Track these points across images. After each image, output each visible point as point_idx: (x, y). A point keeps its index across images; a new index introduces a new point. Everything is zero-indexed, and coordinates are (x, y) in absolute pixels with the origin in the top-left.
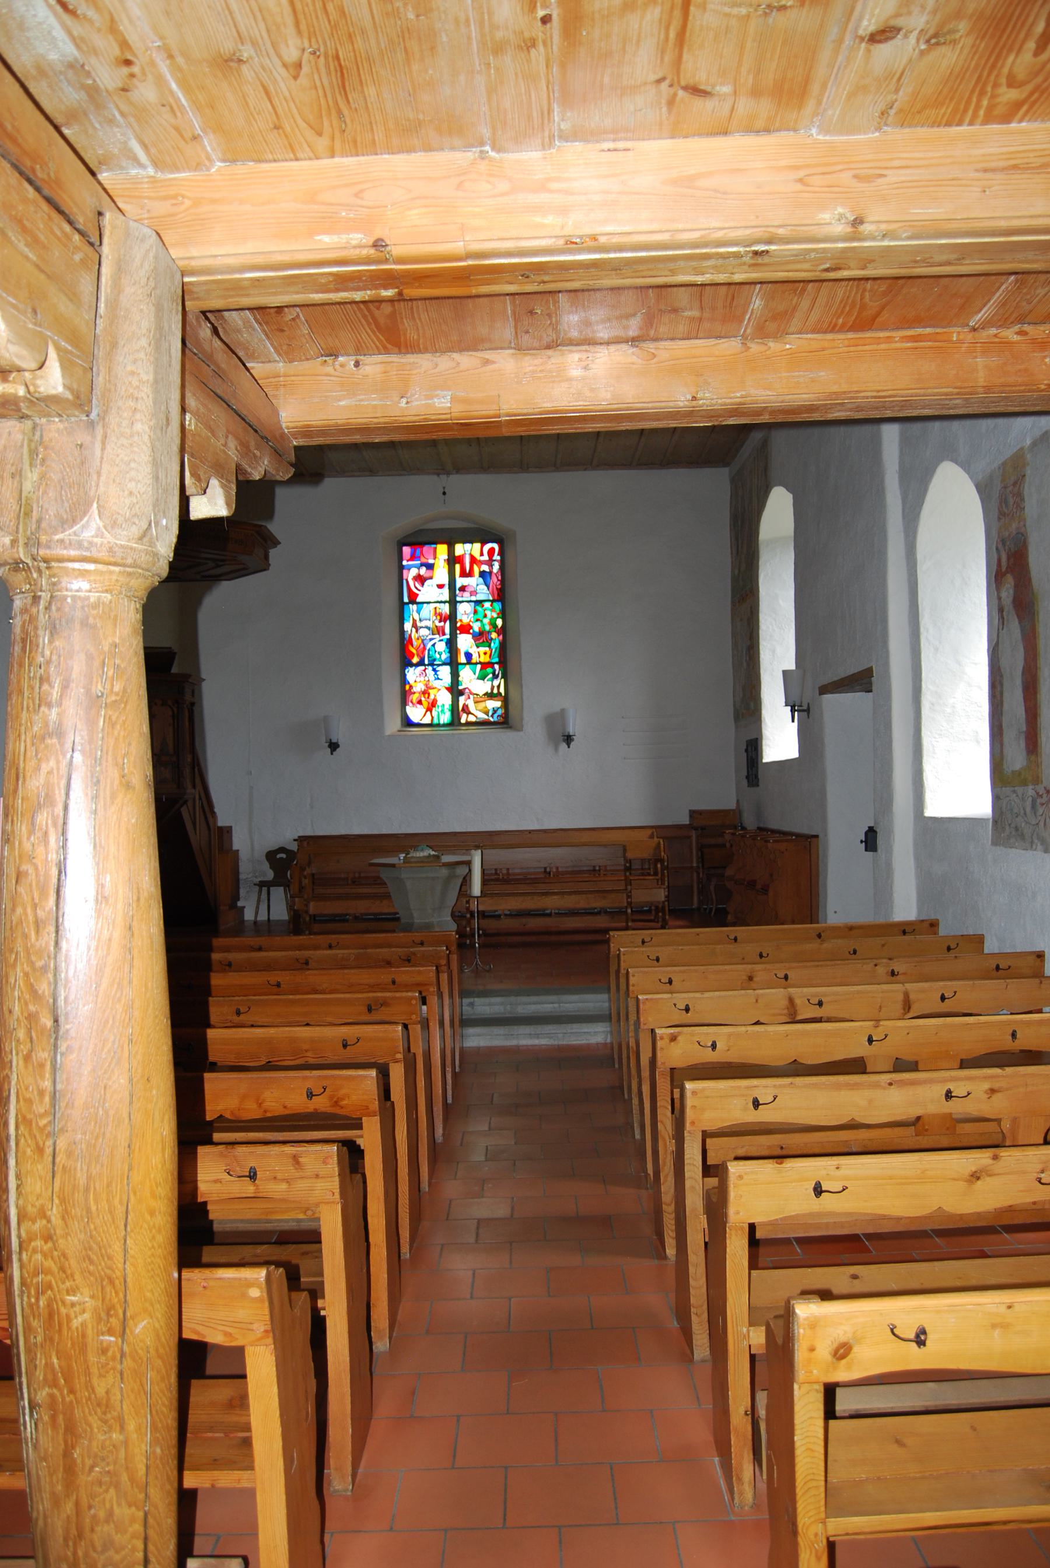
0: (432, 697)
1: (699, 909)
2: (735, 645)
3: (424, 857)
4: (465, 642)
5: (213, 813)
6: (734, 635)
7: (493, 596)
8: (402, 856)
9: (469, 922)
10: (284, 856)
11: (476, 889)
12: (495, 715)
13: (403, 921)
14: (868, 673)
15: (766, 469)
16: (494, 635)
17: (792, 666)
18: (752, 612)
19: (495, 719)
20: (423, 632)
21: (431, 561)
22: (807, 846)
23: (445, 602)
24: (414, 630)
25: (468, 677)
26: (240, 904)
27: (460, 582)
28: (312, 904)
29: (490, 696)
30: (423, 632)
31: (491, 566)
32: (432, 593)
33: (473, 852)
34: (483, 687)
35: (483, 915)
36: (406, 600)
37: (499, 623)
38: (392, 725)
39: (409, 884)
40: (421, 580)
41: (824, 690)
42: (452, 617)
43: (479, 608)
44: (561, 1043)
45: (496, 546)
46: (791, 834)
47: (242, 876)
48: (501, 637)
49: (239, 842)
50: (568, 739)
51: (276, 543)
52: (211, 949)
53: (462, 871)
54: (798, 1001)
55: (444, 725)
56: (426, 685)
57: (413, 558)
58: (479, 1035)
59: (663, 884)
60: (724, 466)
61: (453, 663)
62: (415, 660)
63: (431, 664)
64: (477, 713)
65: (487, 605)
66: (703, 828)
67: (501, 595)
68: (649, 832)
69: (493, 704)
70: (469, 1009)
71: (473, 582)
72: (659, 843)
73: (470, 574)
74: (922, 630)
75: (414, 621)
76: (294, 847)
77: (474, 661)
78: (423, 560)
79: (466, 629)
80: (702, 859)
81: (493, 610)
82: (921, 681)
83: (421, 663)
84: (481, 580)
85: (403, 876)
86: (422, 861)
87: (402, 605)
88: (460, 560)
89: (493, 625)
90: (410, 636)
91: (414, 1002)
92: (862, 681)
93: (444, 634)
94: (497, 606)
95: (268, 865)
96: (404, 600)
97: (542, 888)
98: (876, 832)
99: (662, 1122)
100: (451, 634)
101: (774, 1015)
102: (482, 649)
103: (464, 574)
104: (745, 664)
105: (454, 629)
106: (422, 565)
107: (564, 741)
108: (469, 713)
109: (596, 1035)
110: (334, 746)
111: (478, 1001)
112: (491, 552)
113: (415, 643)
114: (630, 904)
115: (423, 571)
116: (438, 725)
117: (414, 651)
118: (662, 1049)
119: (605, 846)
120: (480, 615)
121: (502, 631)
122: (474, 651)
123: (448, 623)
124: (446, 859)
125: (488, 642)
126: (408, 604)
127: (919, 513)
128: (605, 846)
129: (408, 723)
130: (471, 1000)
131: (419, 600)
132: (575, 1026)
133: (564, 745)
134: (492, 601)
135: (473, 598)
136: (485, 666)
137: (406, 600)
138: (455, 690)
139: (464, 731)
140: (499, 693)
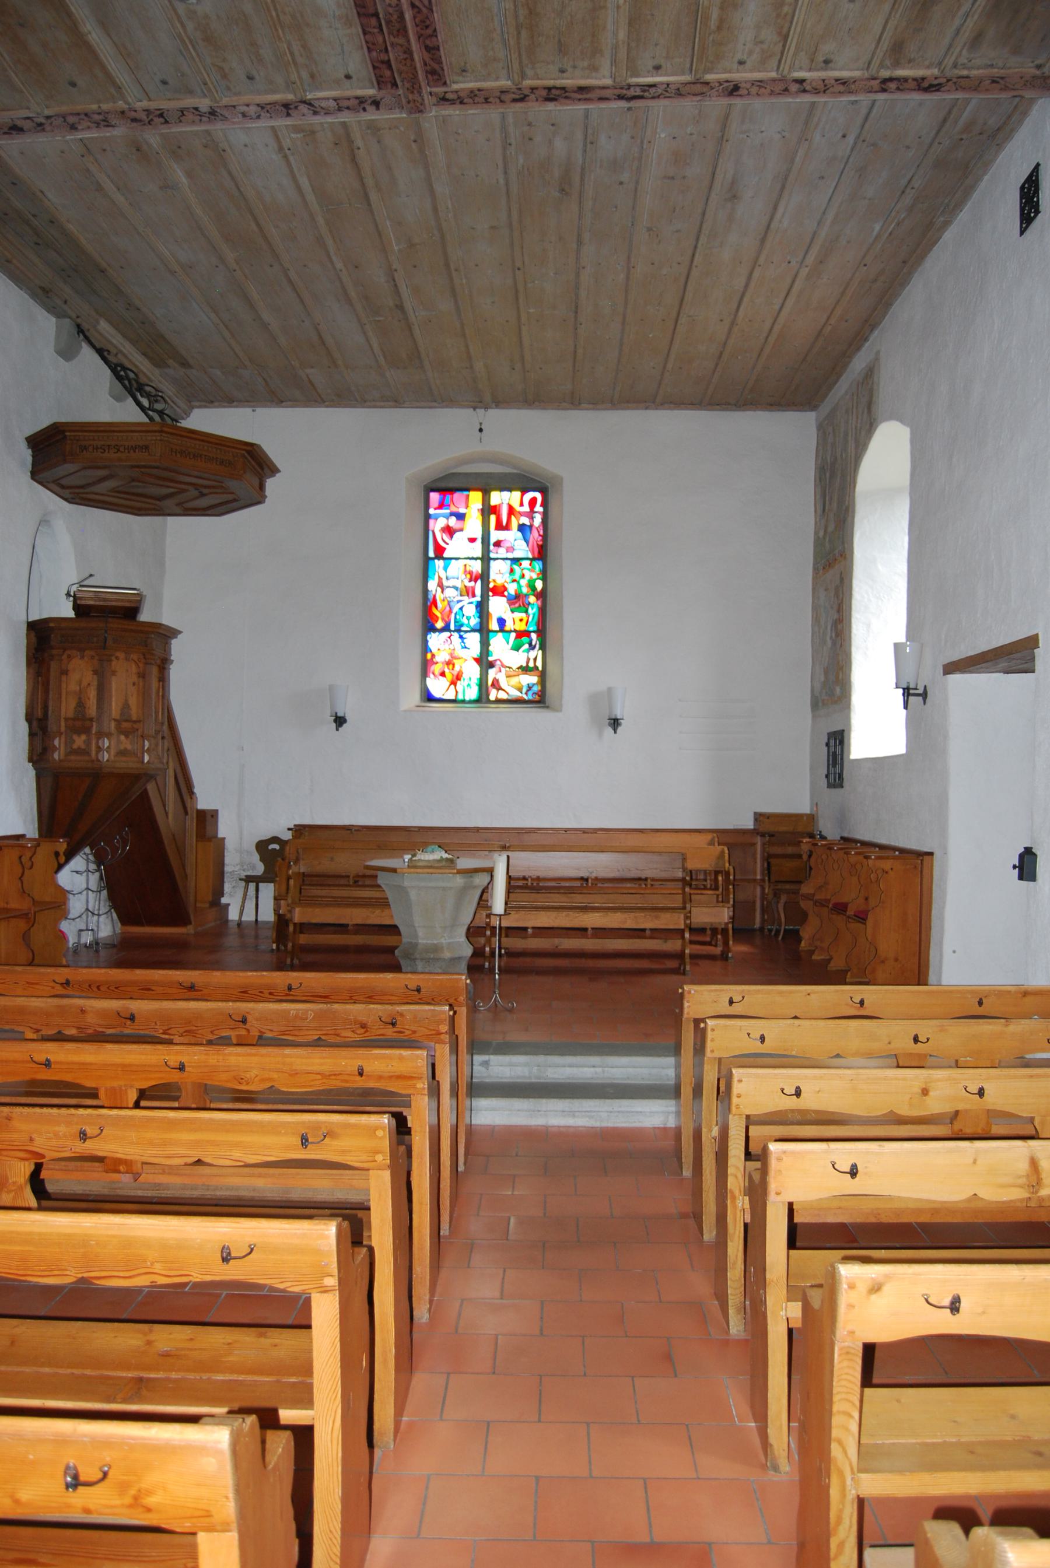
0: (457, 669)
1: (762, 929)
2: (816, 620)
3: (434, 860)
4: (498, 606)
5: (191, 793)
6: (815, 608)
7: (533, 553)
8: (407, 857)
9: (489, 941)
10: (277, 847)
11: (498, 905)
12: (530, 693)
14: (1032, 642)
15: (870, 405)
16: (532, 599)
17: (902, 638)
18: (842, 580)
20: (450, 593)
21: (462, 510)
22: (918, 863)
23: (476, 559)
24: (439, 590)
25: (500, 647)
27: (495, 535)
28: (297, 910)
29: (525, 670)
30: (450, 593)
31: (532, 518)
33: (496, 855)
34: (519, 658)
35: (509, 931)
36: (431, 554)
39: (413, 895)
40: (450, 531)
41: (951, 668)
42: (484, 576)
43: (515, 567)
44: (605, 1124)
45: (538, 496)
46: (894, 849)
47: (227, 869)
48: (539, 602)
49: (225, 829)
50: (615, 723)
51: (274, 470)
52: (240, 924)
53: (481, 880)
55: (470, 702)
56: (451, 655)
57: (441, 506)
58: (494, 1109)
60: (812, 410)
61: (483, 630)
62: (439, 625)
63: (458, 630)
65: (526, 564)
66: (771, 835)
67: (541, 553)
68: (709, 837)
70: (482, 1069)
71: (512, 536)
72: (723, 852)
73: (507, 528)
75: (440, 579)
76: (287, 836)
77: (507, 628)
78: (453, 509)
79: (499, 591)
80: (768, 870)
81: (533, 571)
83: (446, 628)
84: (519, 534)
85: (406, 884)
86: (430, 866)
87: (427, 560)
88: (495, 510)
89: (531, 586)
90: (435, 596)
93: (474, 596)
94: (538, 566)
95: (258, 857)
97: (579, 900)
98: (1035, 855)
99: (840, 1442)
100: (482, 596)
101: (1003, 1186)
102: (518, 615)
103: (499, 527)
104: (829, 642)
105: (486, 590)
106: (452, 514)
107: (610, 725)
109: (654, 1115)
110: (340, 721)
112: (533, 502)
113: (440, 605)
115: (453, 522)
116: (463, 701)
117: (438, 614)
118: (851, 1306)
119: (660, 853)
121: (541, 595)
122: (508, 616)
123: (479, 582)
125: (526, 606)
126: (433, 559)
128: (660, 853)
129: (429, 698)
130: (485, 1058)
131: (445, 555)
133: (610, 730)
134: (531, 560)
135: (510, 555)
136: (520, 634)
137: (431, 554)
138: (485, 662)
140: (536, 668)
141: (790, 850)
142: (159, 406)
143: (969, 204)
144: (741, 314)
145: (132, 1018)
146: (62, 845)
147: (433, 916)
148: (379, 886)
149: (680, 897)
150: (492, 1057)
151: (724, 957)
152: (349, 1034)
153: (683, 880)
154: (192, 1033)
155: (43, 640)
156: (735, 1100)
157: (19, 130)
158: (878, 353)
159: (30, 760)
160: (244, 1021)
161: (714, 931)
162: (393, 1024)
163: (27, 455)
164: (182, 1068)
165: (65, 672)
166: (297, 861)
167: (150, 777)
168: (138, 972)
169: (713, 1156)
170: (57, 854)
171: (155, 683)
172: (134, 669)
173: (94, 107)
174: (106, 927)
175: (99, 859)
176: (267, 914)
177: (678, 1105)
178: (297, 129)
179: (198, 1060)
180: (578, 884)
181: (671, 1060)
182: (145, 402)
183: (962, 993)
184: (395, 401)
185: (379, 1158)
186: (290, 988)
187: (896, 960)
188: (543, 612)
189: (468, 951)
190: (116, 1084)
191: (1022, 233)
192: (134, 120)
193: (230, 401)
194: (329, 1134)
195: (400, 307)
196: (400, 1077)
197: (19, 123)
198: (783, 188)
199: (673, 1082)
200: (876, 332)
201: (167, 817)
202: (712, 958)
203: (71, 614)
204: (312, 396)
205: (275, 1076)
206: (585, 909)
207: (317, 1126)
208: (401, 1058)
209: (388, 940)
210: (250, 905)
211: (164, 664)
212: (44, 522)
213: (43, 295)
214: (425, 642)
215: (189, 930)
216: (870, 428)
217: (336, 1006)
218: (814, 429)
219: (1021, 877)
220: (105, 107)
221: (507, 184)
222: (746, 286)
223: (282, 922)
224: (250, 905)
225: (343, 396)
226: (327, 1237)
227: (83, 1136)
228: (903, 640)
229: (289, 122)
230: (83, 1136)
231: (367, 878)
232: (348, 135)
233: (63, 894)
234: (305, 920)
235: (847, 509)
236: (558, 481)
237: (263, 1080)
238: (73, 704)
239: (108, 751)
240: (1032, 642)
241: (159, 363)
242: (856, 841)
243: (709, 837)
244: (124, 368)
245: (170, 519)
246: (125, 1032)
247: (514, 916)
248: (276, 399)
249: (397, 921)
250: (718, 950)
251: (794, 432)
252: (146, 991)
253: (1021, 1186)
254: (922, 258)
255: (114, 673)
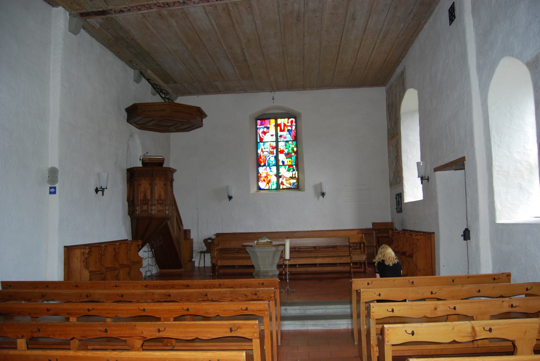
0: (269, 179)
2: (389, 156)
4: (282, 157)
5: (182, 224)
6: (389, 152)
8: (256, 242)
9: (284, 269)
10: (210, 241)
11: (287, 256)
13: (256, 269)
14: (463, 159)
16: (293, 154)
17: (419, 160)
18: (397, 142)
19: (294, 187)
20: (266, 153)
21: (268, 126)
22: (429, 238)
25: (283, 171)
26: (193, 260)
27: (280, 133)
28: (219, 261)
29: (292, 178)
31: (292, 127)
32: (269, 138)
34: (289, 174)
35: (291, 266)
36: (259, 141)
37: (295, 149)
38: (254, 189)
39: (258, 254)
40: (264, 133)
41: (436, 170)
42: (277, 147)
43: (287, 144)
44: (327, 328)
45: (294, 120)
46: (421, 232)
47: (194, 249)
49: (193, 236)
50: (323, 194)
52: (199, 268)
54: (477, 329)
57: (261, 125)
59: (364, 252)
61: (277, 165)
62: (262, 164)
63: (269, 166)
64: (287, 185)
65: (290, 142)
66: (378, 230)
68: (357, 231)
69: (293, 181)
70: (285, 311)
71: (285, 133)
73: (284, 131)
74: (492, 137)
76: (214, 237)
79: (282, 152)
82: (492, 160)
83: (265, 165)
85: (256, 250)
86: (264, 244)
87: (257, 143)
88: (280, 125)
89: (293, 150)
91: (255, 327)
92: (459, 164)
94: (294, 143)
96: (258, 141)
97: (313, 255)
98: (469, 231)
103: (281, 131)
104: (394, 164)
106: (265, 127)
108: (283, 185)
109: (344, 325)
110: (230, 198)
111: (288, 308)
112: (292, 122)
113: (262, 157)
114: (351, 261)
115: (265, 130)
116: (272, 189)
120: (288, 147)
121: (296, 153)
124: (275, 243)
127: (489, 84)
128: (341, 237)
129: (260, 189)
130: (286, 307)
132: (334, 321)
133: (322, 197)
135: (285, 140)
136: (290, 166)
137: (259, 141)
138: (278, 176)
139: (281, 192)
140: (295, 177)
141: (385, 235)
142: (168, 97)
143: (432, 17)
144: (358, 56)
145: (169, 296)
146: (140, 242)
147: (265, 261)
148: (247, 252)
149: (348, 252)
150: (288, 307)
151: (365, 272)
152: (241, 298)
153: (349, 247)
154: (189, 299)
155: (132, 175)
156: (372, 314)
157: (122, 11)
158: (405, 66)
159: (129, 214)
160: (206, 295)
161: (361, 263)
162: (256, 295)
163: (125, 114)
164: (188, 310)
165: (140, 185)
166: (218, 245)
167: (169, 219)
168: (170, 281)
169: (365, 336)
170: (138, 245)
171: (169, 187)
172: (162, 183)
173: (146, 3)
174: (155, 270)
175: (152, 247)
176: (208, 264)
177: (352, 321)
178: (211, 6)
179: (193, 307)
180: (313, 249)
181: (349, 306)
182: (163, 96)
183: (447, 278)
184: (245, 91)
185: (256, 335)
186: (220, 285)
187: (424, 270)
188: (297, 158)
189: (277, 273)
190: (166, 316)
191: (450, 25)
192: (159, 6)
193: (190, 94)
194: (239, 327)
195: (246, 60)
196: (260, 310)
197: (122, 9)
198: (370, 15)
199: (350, 313)
200: (404, 59)
201: (174, 232)
202: (361, 272)
203: (141, 166)
204: (217, 91)
205: (219, 311)
206: (316, 257)
207: (235, 325)
208: (260, 304)
209: (250, 270)
210: (204, 261)
211: (172, 181)
212: (132, 136)
213: (130, 63)
214: (258, 170)
215: (182, 270)
216: (404, 91)
217: (237, 289)
218: (385, 93)
219: (465, 239)
220: (150, 3)
221: (279, 18)
222: (360, 47)
223: (214, 266)
224: (204, 261)
225: (227, 90)
226: (242, 356)
227: (159, 331)
228: (419, 161)
229: (208, 4)
230: (159, 331)
231: (243, 249)
232: (227, 6)
233: (141, 259)
234: (222, 265)
235: (398, 118)
236: (300, 114)
237: (215, 313)
238: (142, 195)
239: (155, 210)
240: (463, 159)
241: (167, 82)
242: (408, 230)
243: (357, 231)
244: (156, 85)
245: (171, 134)
246: (168, 299)
247: (292, 260)
248: (205, 92)
249: (254, 263)
250: (363, 270)
251: (378, 94)
252: (173, 287)
253: (469, 337)
254: (418, 34)
255: (156, 184)
